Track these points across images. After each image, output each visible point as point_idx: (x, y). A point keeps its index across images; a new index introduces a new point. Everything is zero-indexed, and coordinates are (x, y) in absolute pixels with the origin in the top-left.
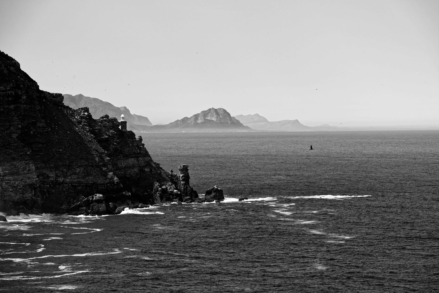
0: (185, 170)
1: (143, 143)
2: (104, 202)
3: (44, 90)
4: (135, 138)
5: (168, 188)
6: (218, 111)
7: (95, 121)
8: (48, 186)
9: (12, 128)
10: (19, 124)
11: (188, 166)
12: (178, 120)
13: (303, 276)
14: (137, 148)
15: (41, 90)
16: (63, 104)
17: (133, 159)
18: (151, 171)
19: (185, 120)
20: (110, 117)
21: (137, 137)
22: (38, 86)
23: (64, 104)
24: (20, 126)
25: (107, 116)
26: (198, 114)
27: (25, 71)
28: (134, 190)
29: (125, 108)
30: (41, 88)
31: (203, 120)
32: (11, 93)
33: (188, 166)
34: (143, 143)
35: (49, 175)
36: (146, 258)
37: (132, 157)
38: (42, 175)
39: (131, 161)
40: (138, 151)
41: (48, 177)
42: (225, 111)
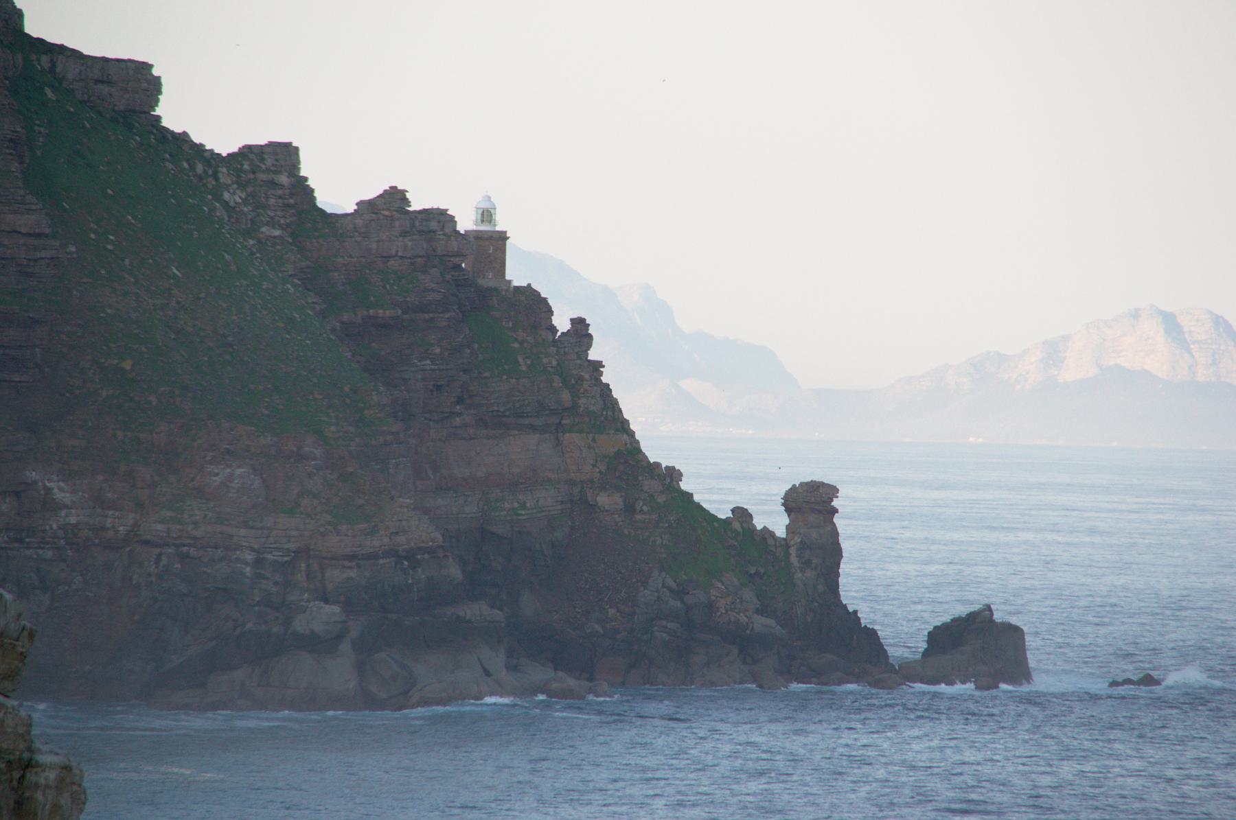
0: (812, 503)
1: (593, 355)
2: (345, 647)
3: (53, 36)
4: (553, 329)
5: (722, 603)
8: (49, 554)
11: (832, 491)
13: (1207, 697)
14: (557, 383)
16: (158, 118)
17: (533, 439)
18: (630, 509)
21: (562, 323)
25: (395, 197)
28: (529, 605)
33: (832, 491)
34: (593, 355)
35: (58, 495)
36: (315, 717)
37: (533, 428)
38: (17, 494)
39: (520, 450)
40: (566, 396)
41: (49, 505)
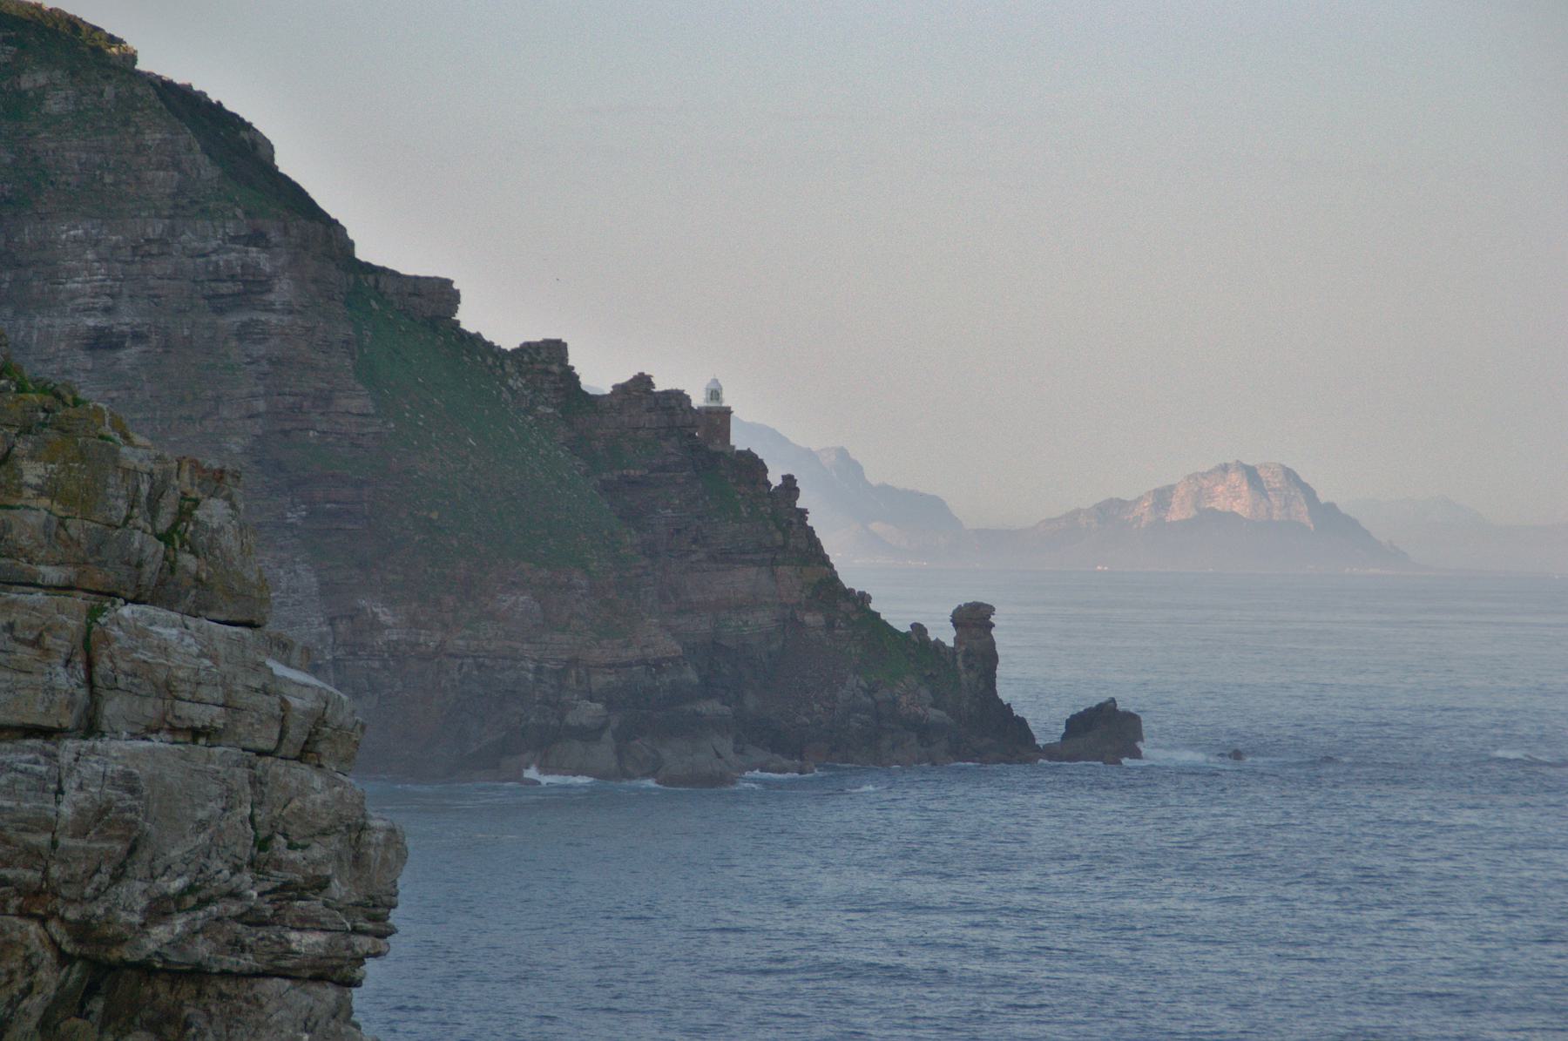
1: (800, 504)
5: (904, 700)
6: (1262, 473)
7: (593, 401)
8: (377, 665)
9: (225, 413)
10: (253, 396)
11: (990, 610)
12: (1079, 511)
14: (772, 527)
15: (363, 259)
16: (458, 323)
19: (1110, 511)
20: (660, 385)
21: (775, 479)
22: (352, 244)
23: (463, 326)
24: (261, 406)
25: (643, 381)
26: (1172, 488)
27: (295, 176)
28: (751, 702)
29: (842, 454)
30: (361, 254)
31: (1193, 513)
32: (227, 262)
33: (990, 610)
34: (800, 504)
35: (382, 618)
38: (351, 618)
40: (779, 537)
41: (376, 626)
42: (1289, 474)
